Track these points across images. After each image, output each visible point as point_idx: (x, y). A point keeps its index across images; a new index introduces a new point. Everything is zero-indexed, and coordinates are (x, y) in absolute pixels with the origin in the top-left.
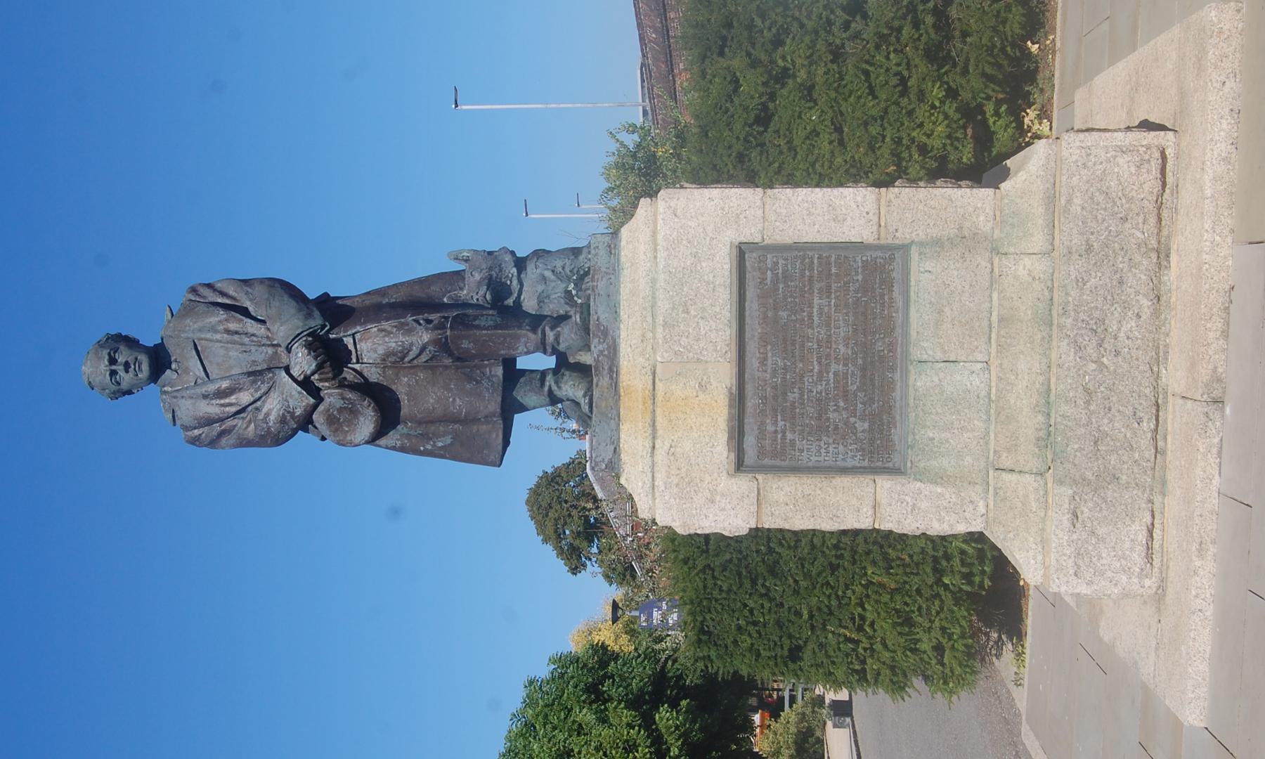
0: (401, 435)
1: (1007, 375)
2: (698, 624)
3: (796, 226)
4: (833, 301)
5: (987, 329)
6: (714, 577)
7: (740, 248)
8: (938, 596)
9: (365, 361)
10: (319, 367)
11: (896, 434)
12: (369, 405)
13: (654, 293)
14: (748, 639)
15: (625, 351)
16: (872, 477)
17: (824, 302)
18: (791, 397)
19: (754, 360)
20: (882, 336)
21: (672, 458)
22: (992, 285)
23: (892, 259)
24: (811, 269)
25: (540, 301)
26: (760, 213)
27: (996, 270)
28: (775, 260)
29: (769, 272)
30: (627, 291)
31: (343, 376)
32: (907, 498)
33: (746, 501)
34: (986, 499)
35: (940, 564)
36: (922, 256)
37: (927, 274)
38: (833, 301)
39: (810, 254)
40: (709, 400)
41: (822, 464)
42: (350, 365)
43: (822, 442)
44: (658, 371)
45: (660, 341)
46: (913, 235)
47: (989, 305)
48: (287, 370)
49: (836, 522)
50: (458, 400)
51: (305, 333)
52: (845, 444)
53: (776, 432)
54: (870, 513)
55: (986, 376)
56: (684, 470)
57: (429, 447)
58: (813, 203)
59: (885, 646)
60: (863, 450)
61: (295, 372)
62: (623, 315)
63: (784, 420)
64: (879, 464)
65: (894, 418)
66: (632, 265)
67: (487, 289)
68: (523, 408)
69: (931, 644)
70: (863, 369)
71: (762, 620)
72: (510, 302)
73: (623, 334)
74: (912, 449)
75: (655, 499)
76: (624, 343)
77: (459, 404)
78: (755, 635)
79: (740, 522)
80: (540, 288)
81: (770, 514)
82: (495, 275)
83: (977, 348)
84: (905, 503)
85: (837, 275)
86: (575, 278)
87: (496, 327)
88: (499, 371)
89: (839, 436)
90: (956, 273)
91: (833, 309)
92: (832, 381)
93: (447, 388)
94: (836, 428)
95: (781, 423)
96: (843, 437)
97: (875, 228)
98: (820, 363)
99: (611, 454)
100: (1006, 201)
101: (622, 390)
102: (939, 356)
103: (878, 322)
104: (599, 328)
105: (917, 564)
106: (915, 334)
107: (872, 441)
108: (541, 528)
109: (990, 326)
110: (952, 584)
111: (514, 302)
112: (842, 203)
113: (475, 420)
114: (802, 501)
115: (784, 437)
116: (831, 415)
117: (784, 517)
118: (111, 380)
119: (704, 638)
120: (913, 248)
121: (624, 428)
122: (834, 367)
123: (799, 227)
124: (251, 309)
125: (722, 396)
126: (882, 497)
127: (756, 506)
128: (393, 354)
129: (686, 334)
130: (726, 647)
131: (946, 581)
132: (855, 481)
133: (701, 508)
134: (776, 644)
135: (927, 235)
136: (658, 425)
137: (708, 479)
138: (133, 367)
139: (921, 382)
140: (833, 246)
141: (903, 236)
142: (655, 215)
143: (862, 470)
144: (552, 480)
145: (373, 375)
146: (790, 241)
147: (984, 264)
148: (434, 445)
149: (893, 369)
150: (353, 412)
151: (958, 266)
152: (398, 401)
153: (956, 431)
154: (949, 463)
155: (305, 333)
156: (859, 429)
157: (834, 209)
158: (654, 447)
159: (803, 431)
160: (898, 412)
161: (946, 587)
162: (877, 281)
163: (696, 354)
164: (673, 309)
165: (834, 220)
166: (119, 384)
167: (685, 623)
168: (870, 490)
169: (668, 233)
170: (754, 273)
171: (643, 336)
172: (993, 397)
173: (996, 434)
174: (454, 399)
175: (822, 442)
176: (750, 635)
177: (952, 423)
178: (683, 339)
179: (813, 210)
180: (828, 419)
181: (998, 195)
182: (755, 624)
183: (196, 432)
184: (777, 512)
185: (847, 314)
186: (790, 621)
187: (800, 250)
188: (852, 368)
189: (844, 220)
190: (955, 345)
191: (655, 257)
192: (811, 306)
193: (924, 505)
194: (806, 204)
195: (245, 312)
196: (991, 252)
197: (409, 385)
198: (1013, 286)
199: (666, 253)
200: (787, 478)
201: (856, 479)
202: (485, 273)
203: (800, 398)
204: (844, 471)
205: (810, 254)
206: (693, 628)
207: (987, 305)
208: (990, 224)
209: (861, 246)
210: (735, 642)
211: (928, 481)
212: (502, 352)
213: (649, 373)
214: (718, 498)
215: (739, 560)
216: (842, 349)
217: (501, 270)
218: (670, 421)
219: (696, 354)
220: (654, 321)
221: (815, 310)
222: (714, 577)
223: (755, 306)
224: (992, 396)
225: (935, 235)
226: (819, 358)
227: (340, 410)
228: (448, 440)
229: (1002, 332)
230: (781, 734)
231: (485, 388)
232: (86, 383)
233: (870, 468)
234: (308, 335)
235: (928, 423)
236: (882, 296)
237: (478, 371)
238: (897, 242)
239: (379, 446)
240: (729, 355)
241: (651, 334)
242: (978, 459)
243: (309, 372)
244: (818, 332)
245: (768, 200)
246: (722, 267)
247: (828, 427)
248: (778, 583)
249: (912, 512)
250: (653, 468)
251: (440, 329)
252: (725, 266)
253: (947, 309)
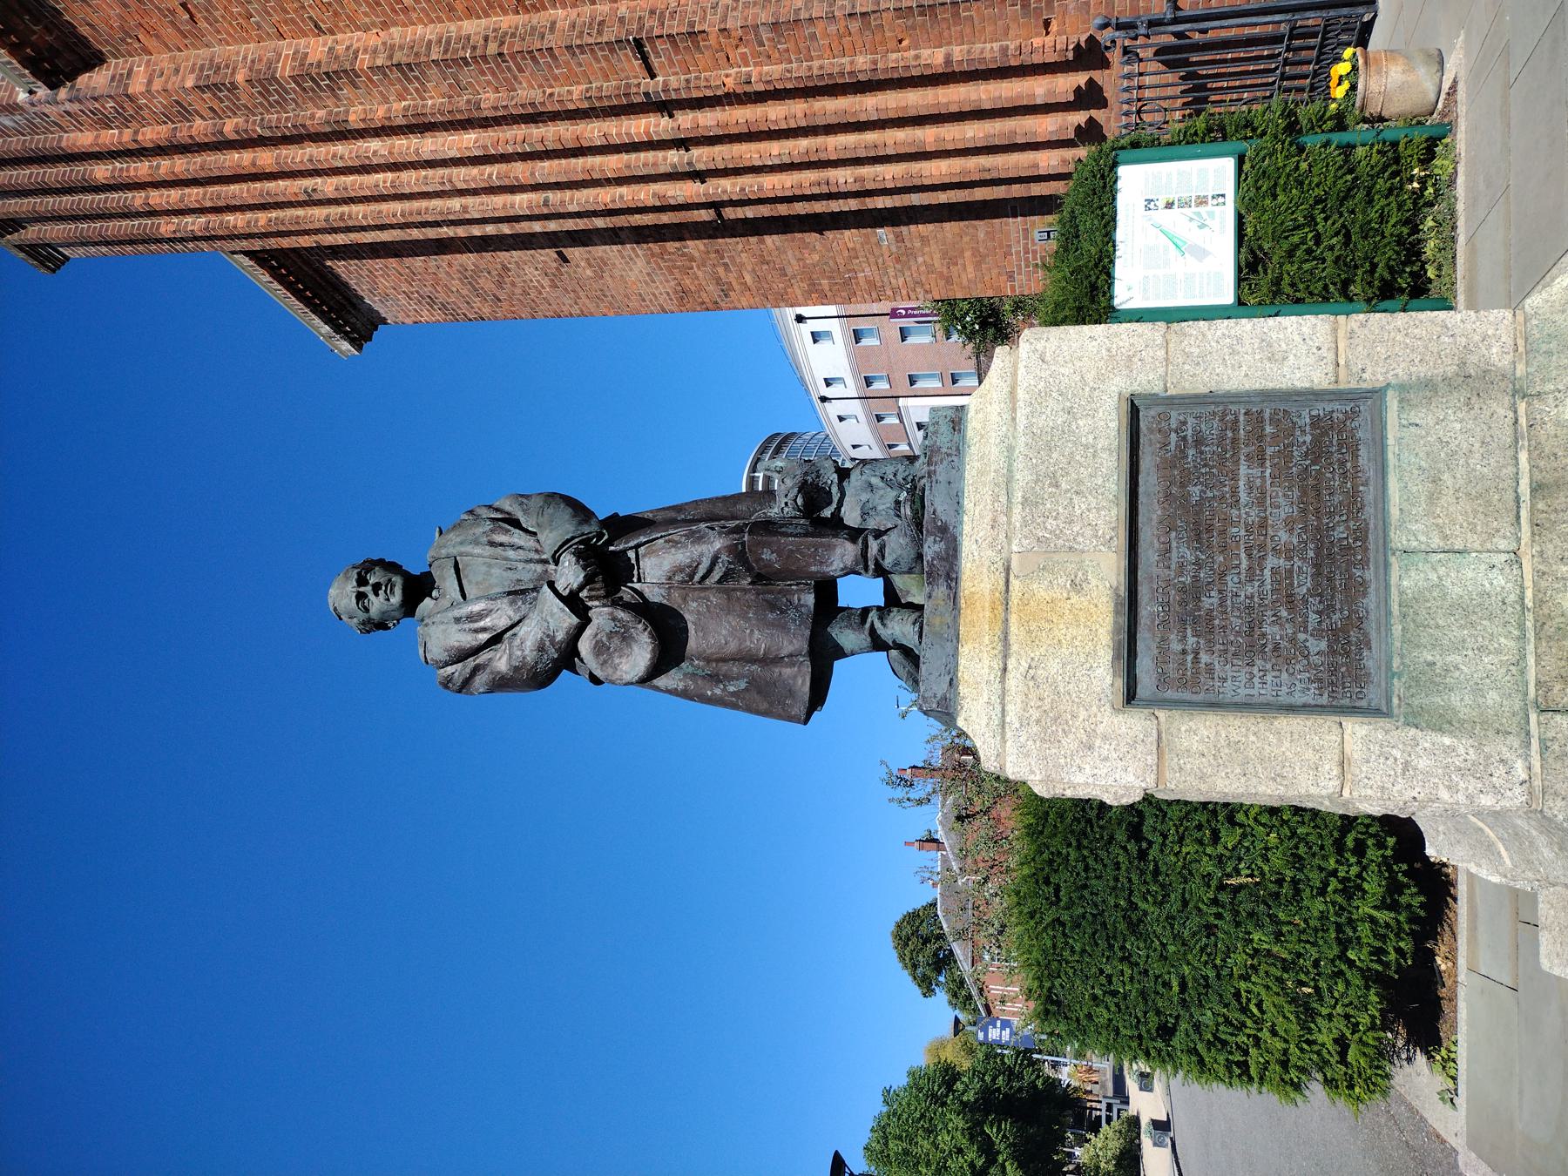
0: (685, 675)
1: (1554, 567)
2: (1045, 990)
3: (1214, 369)
4: (1268, 471)
5: (1512, 504)
6: (1064, 934)
7: (1132, 401)
8: (1341, 973)
9: (648, 580)
10: (588, 580)
11: (1370, 661)
12: (645, 629)
13: (1010, 465)
14: (1105, 1012)
15: (968, 548)
16: (1337, 719)
17: (1256, 472)
18: (1206, 602)
19: (1150, 552)
20: (1344, 518)
21: (1031, 684)
22: (1517, 442)
23: (1354, 414)
24: (1235, 430)
25: (865, 514)
26: (1161, 353)
27: (1523, 421)
28: (1181, 418)
29: (1173, 435)
30: (974, 472)
31: (619, 595)
32: (1394, 752)
33: (1140, 748)
34: (1527, 757)
35: (1344, 932)
36: (1404, 404)
37: (1412, 429)
38: (1268, 471)
39: (1233, 408)
40: (1085, 604)
41: (1255, 700)
42: (629, 584)
43: (1256, 669)
44: (1014, 565)
45: (1018, 525)
46: (1389, 376)
47: (1515, 470)
48: (551, 585)
49: (1282, 785)
50: (756, 632)
51: (577, 540)
52: (1291, 671)
53: (1184, 652)
54: (1335, 773)
55: (1515, 572)
56: (1048, 701)
57: (718, 692)
58: (1239, 339)
59: (1274, 1033)
60: (1320, 680)
61: (560, 587)
62: (968, 504)
63: (1196, 636)
64: (1346, 702)
65: (1366, 635)
66: (982, 437)
67: (799, 492)
68: (840, 653)
69: (1331, 1036)
70: (1318, 566)
71: (1122, 991)
72: (827, 513)
73: (967, 528)
74: (1399, 679)
75: (1005, 742)
76: (968, 539)
77: (758, 640)
78: (1113, 1009)
79: (1130, 778)
80: (864, 497)
81: (1176, 768)
82: (810, 480)
83: (1498, 531)
84: (1392, 759)
85: (1274, 436)
86: (908, 486)
87: (806, 535)
88: (810, 599)
89: (1281, 660)
90: (1458, 426)
91: (1268, 482)
92: (1269, 581)
93: (744, 617)
94: (1276, 648)
95: (1191, 640)
96: (1288, 662)
97: (1330, 368)
98: (1250, 556)
99: (945, 686)
100: (1535, 322)
101: (963, 601)
102: (1436, 542)
103: (1337, 498)
104: (935, 523)
105: (1316, 930)
106: (1398, 513)
107: (1333, 670)
108: (902, 957)
109: (1517, 499)
110: (1359, 959)
111: (832, 514)
112: (1282, 336)
113: (778, 660)
114: (1227, 751)
115: (1196, 659)
116: (1268, 629)
117: (1200, 774)
118: (358, 604)
119: (1053, 1008)
120: (1390, 393)
121: (964, 650)
122: (1271, 562)
123: (1218, 371)
124: (522, 520)
125: (1105, 599)
126: (1354, 748)
127: (1155, 757)
128: (680, 569)
129: (1054, 514)
130: (1078, 1020)
131: (1351, 955)
132: (1309, 723)
133: (1072, 755)
134: (1139, 1021)
135: (1411, 375)
136: (1012, 638)
137: (1083, 714)
138: (384, 588)
139: (1406, 580)
140: (1267, 395)
141: (1374, 376)
142: (1015, 367)
143: (1320, 709)
144: (913, 917)
145: (654, 595)
146: (1203, 390)
147: (1501, 412)
148: (724, 690)
149: (1364, 564)
150: (626, 638)
151: (1460, 416)
152: (686, 630)
153: (1470, 653)
154: (1462, 700)
155: (577, 540)
156: (1313, 649)
157: (1270, 345)
158: (1005, 670)
159: (1226, 651)
160: (1373, 625)
161: (1351, 963)
162: (1335, 443)
163: (1068, 540)
164: (1036, 482)
165: (1269, 359)
166: (367, 610)
167: (1030, 991)
168: (1334, 738)
169: (1032, 383)
170: (1152, 436)
171: (994, 521)
172: (1529, 603)
173: (1537, 655)
174: (752, 631)
175: (1256, 669)
176: (1107, 1008)
177: (1464, 641)
178: (1050, 521)
179: (1238, 348)
180: (1264, 635)
181: (1520, 318)
182: (1114, 993)
183: (450, 669)
184: (1189, 766)
185: (1290, 488)
186: (1157, 993)
187: (1216, 403)
188: (1300, 563)
189: (1284, 359)
190: (1461, 527)
191: (1014, 419)
192: (1235, 478)
193: (1423, 763)
194: (1228, 340)
195: (516, 523)
196: (1513, 396)
197: (698, 611)
198: (1556, 436)
199: (1028, 410)
200: (1203, 717)
201: (1312, 721)
202: (799, 479)
203: (1221, 605)
204: (1291, 709)
205: (1233, 408)
206: (1040, 996)
207: (1511, 470)
208: (1509, 358)
209: (1315, 395)
210: (1089, 1016)
211: (1428, 727)
212: (813, 569)
213: (1001, 570)
214: (1098, 742)
215: (1094, 916)
216: (1283, 536)
217: (818, 477)
218: (1029, 632)
219: (1068, 540)
220: (1009, 500)
221: (1241, 483)
222: (1064, 934)
223: (1153, 479)
224: (1526, 601)
225: (1422, 375)
226: (1248, 550)
227: (611, 635)
228: (743, 685)
229: (1541, 506)
230: (1101, 1149)
231: (791, 618)
232: (332, 609)
233: (1332, 706)
234: (580, 543)
235: (1423, 641)
236: (1342, 463)
237: (784, 600)
238: (1364, 386)
239: (657, 688)
240: (1115, 542)
241: (1005, 519)
242: (1510, 694)
243: (575, 586)
244: (1246, 513)
245: (1173, 338)
246: (1108, 426)
247: (1264, 645)
248: (1142, 945)
249: (1404, 774)
250: (1003, 699)
251: (737, 533)
252: (1110, 425)
253: (1445, 477)
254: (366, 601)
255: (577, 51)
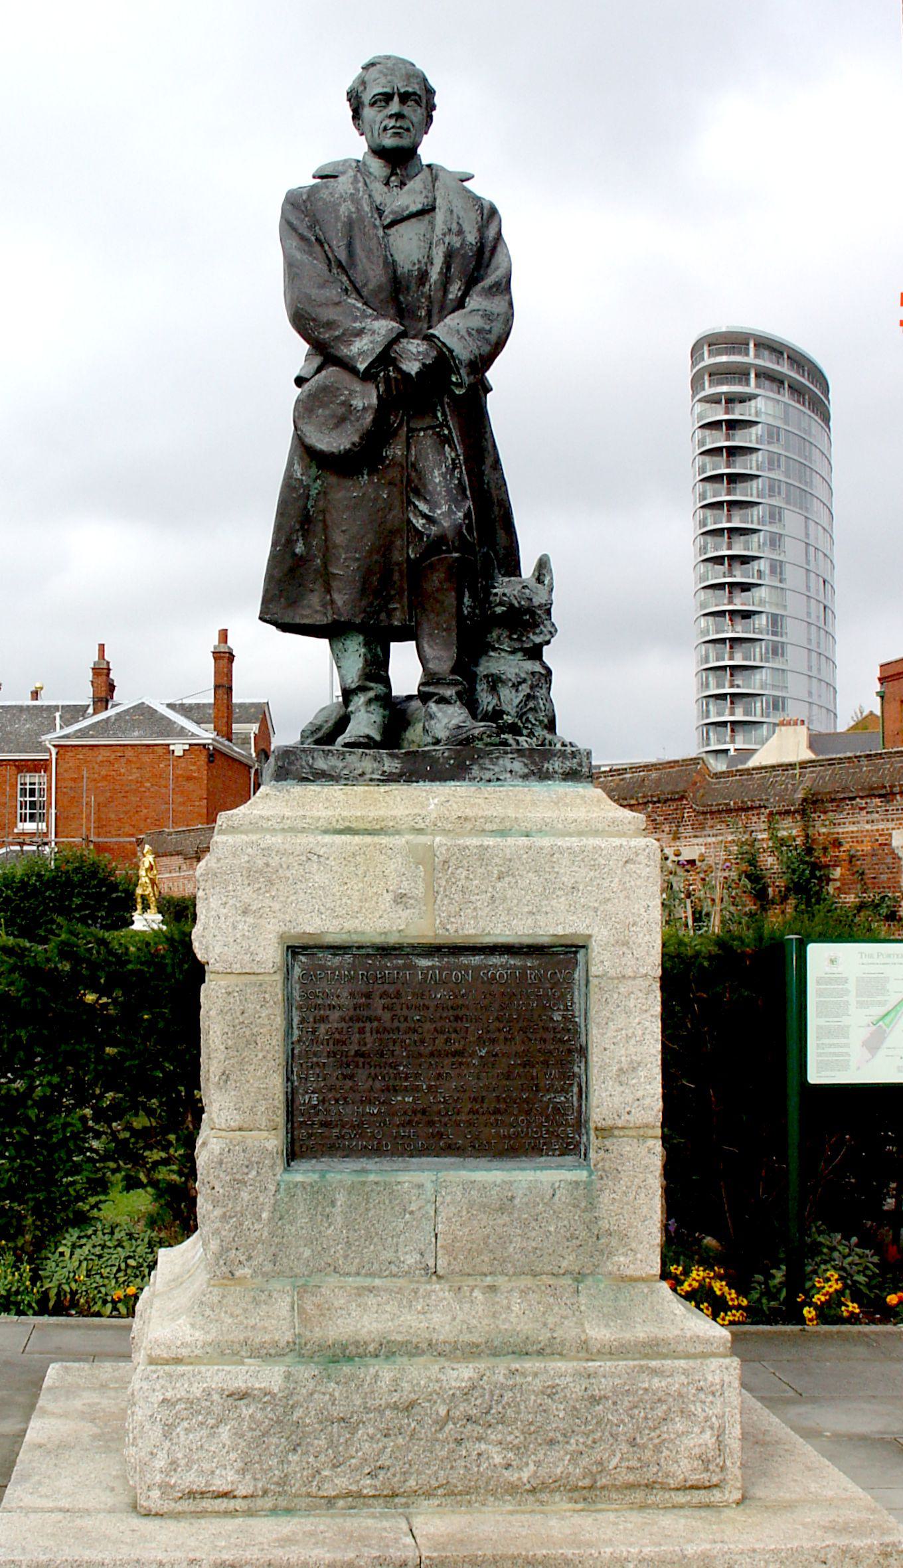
254: (383, 104)
255: (531, 705)
